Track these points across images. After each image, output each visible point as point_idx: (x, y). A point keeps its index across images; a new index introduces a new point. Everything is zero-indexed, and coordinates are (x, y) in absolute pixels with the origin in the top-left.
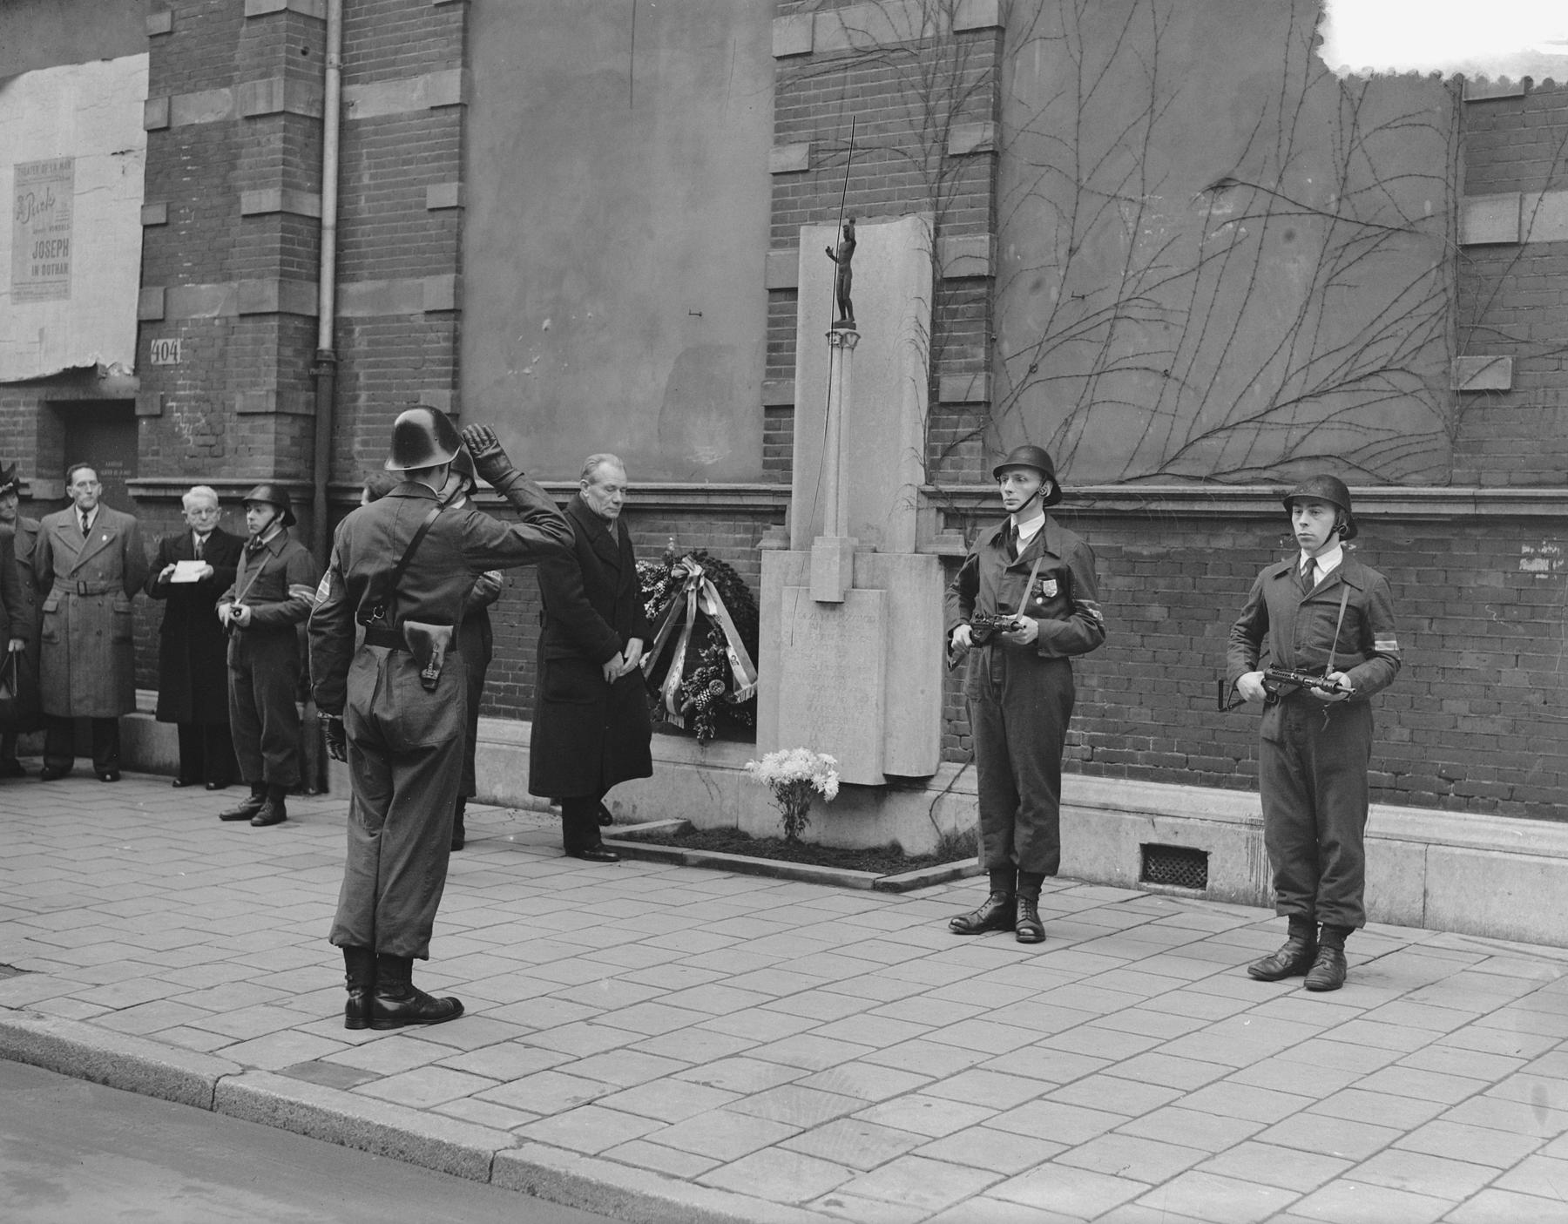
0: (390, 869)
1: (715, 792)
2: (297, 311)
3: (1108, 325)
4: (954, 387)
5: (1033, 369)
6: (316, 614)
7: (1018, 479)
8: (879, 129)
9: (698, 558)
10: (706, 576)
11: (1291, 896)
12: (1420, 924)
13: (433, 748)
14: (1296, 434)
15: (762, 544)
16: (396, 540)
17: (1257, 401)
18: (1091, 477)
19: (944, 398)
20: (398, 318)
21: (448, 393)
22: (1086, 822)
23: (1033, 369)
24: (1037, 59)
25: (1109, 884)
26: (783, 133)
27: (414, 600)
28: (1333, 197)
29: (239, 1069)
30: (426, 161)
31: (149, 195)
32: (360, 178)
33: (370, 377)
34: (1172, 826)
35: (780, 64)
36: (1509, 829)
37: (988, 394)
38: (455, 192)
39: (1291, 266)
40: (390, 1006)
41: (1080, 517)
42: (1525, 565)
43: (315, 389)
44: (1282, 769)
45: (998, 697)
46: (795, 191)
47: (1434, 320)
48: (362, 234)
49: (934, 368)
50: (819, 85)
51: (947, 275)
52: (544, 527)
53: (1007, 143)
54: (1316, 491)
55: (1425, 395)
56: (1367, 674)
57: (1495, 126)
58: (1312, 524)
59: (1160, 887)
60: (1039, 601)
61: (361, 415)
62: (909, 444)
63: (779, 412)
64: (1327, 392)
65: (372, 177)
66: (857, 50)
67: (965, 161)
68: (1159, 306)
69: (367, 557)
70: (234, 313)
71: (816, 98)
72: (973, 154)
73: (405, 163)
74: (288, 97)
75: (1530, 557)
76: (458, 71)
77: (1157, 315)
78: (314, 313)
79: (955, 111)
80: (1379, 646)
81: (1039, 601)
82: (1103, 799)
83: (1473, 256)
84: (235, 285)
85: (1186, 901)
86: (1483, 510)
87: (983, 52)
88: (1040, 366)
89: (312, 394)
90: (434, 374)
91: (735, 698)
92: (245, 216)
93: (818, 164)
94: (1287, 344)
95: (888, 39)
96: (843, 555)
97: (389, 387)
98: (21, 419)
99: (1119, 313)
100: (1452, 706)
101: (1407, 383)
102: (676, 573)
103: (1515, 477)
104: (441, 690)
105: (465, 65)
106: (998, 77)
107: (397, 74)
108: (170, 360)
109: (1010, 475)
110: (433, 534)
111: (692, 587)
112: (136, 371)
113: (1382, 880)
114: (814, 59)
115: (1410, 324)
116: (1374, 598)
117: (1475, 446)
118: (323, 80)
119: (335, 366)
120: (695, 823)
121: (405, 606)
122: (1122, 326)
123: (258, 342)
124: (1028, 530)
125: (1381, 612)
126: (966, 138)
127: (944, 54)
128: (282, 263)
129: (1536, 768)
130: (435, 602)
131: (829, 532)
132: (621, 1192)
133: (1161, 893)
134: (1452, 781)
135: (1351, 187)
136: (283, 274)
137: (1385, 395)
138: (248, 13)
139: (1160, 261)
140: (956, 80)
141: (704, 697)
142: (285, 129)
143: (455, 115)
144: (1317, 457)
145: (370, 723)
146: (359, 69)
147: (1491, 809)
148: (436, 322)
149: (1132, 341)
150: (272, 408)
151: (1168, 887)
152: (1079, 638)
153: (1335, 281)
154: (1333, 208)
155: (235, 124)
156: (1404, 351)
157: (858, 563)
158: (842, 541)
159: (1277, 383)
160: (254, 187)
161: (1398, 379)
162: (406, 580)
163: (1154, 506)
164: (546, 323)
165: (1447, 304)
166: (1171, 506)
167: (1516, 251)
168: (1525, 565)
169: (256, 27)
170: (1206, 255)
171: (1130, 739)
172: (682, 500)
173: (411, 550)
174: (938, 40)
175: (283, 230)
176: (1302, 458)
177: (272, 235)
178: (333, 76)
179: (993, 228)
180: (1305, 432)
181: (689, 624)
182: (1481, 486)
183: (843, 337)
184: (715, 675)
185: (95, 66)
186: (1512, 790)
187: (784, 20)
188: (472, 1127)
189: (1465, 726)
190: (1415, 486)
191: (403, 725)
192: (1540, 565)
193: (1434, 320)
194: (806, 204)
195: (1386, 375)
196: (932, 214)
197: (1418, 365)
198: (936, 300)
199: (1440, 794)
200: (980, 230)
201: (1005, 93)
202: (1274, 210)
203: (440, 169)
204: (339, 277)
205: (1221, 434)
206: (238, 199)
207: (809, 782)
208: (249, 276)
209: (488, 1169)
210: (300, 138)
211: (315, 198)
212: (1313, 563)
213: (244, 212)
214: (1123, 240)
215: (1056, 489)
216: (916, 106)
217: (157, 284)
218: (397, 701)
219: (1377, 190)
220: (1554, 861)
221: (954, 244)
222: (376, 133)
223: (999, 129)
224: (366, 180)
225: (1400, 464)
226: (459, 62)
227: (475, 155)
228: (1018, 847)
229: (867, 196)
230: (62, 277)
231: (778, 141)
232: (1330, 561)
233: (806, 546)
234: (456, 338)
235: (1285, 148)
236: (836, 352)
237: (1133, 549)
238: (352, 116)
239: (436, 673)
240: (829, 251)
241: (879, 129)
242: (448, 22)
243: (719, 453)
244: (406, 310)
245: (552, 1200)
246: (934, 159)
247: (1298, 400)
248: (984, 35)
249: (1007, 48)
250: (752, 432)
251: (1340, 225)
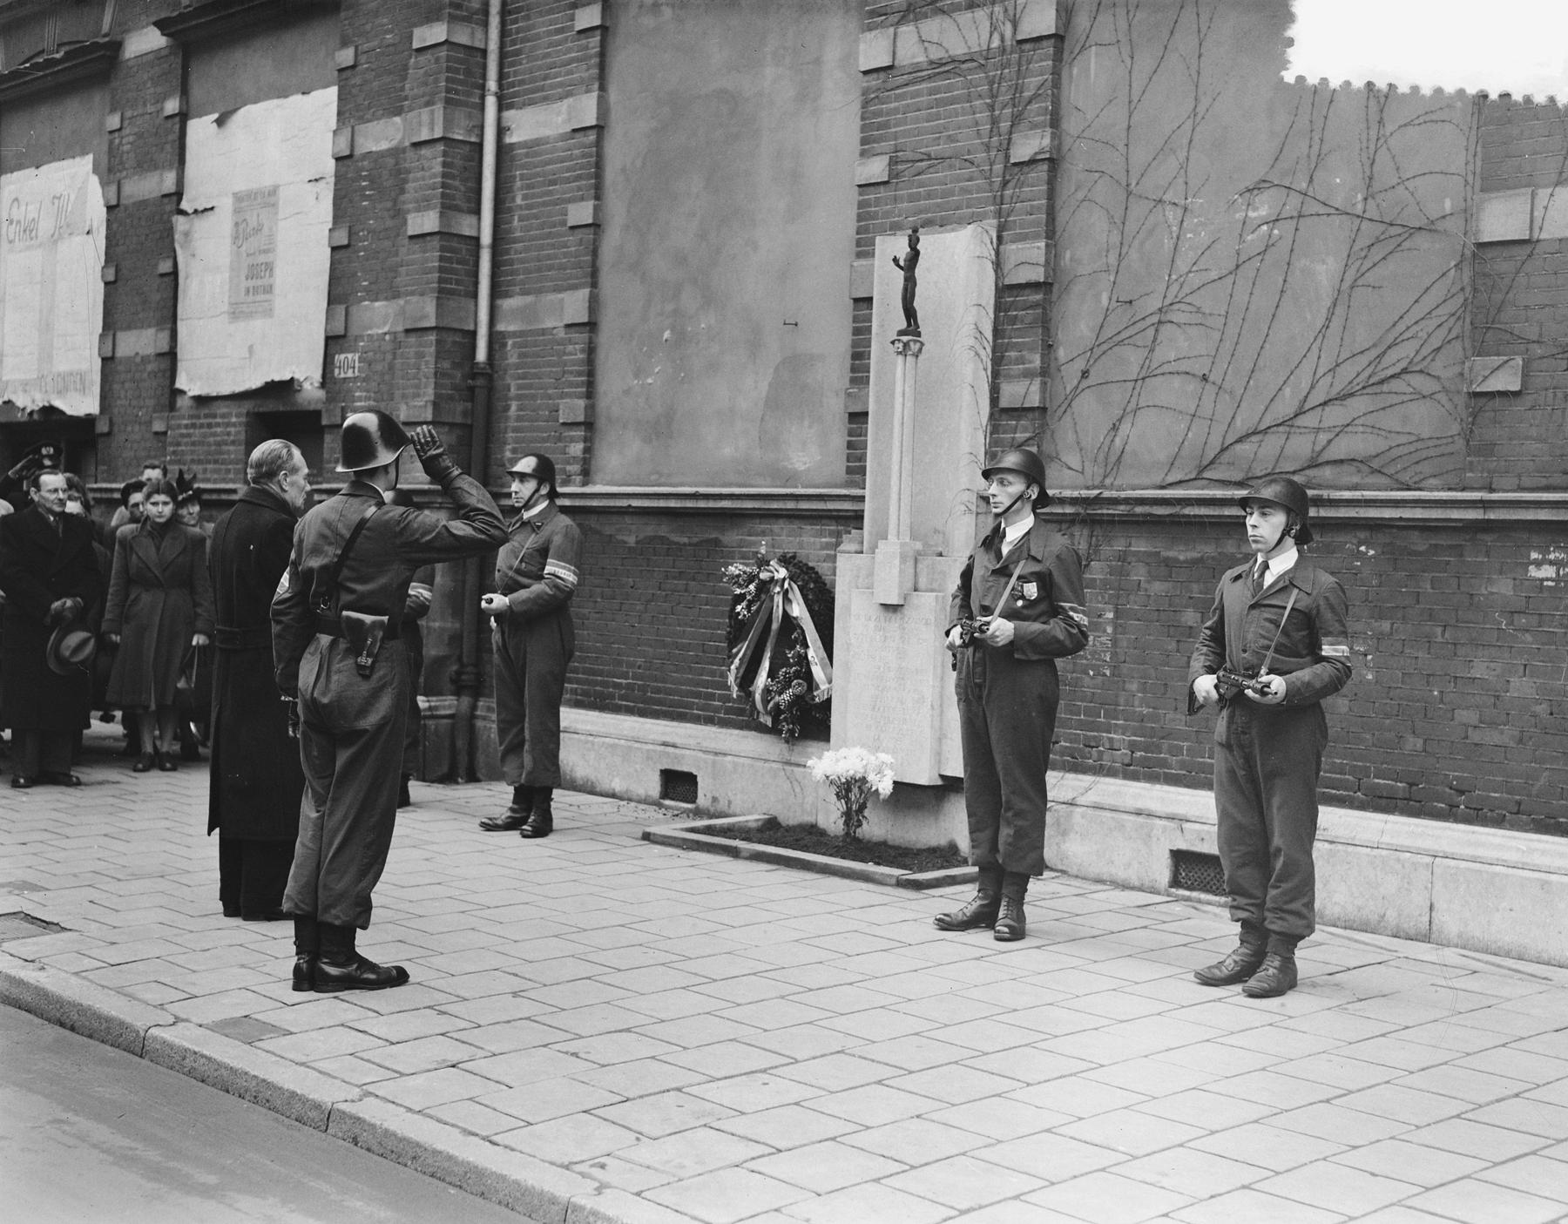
0: (330, 844)
1: (798, 790)
2: (456, 325)
3: (1151, 332)
4: (1013, 393)
5: (1085, 374)
6: (278, 603)
7: (1001, 482)
8: (951, 139)
9: (785, 561)
10: (791, 578)
11: (1242, 901)
12: (1425, 937)
13: (366, 731)
14: (1323, 438)
15: (842, 547)
16: (337, 534)
17: (1285, 408)
18: (1136, 482)
19: (1004, 403)
20: (543, 332)
21: (581, 403)
22: (1121, 827)
23: (1085, 374)
24: (1093, 66)
25: (1140, 889)
26: (867, 146)
27: (352, 591)
28: (1360, 197)
29: (172, 1020)
30: (568, 180)
31: (337, 218)
32: (513, 199)
33: (519, 387)
34: (1199, 832)
35: (867, 78)
36: (1514, 843)
37: (1043, 399)
38: (591, 210)
39: (1321, 268)
40: (333, 971)
41: (1121, 522)
42: (1534, 572)
43: (472, 399)
44: (1232, 773)
45: (980, 697)
46: (877, 202)
47: (1453, 320)
48: (517, 252)
49: (996, 375)
50: (898, 98)
51: (1007, 282)
52: (477, 524)
53: (1065, 148)
54: (1268, 493)
55: (1442, 397)
56: (1307, 679)
57: (1509, 122)
58: (1265, 526)
59: (1187, 893)
60: (1020, 603)
61: (512, 424)
62: (968, 450)
63: (858, 418)
64: (1352, 395)
65: (525, 197)
66: (932, 62)
67: (1026, 169)
68: (1199, 310)
69: (316, 551)
70: (400, 328)
71: (896, 111)
72: (1033, 162)
73: (553, 183)
74: (448, 123)
75: (1538, 564)
76: (595, 94)
77: (1197, 318)
78: (471, 328)
79: (1016, 120)
80: (1327, 650)
81: (1020, 603)
82: (1140, 804)
83: (1489, 253)
84: (401, 302)
85: (1209, 908)
86: (1492, 515)
87: (1042, 62)
88: (1092, 372)
89: (469, 405)
90: (571, 385)
91: (813, 698)
92: (411, 237)
93: (897, 176)
94: (1315, 348)
95: (959, 50)
96: (903, 559)
97: (534, 397)
98: (232, 430)
99: (1164, 318)
100: (1464, 716)
101: (1426, 385)
102: (764, 576)
103: (1526, 482)
104: (375, 677)
105: (602, 88)
106: (1057, 84)
107: (545, 99)
108: (350, 374)
109: (995, 478)
110: (369, 529)
111: (778, 589)
112: (323, 385)
113: (1334, 889)
114: (895, 72)
115: (1431, 324)
116: (1322, 603)
117: (1487, 449)
118: (482, 107)
119: (490, 378)
120: (781, 819)
121: (346, 598)
122: (1166, 330)
123: (420, 355)
124: (1014, 532)
125: (1328, 615)
126: (1027, 146)
127: (1007, 65)
128: (441, 280)
129: (1542, 781)
130: (371, 593)
131: (892, 537)
132: (418, 1145)
133: (1188, 899)
134: (1462, 792)
135: (1376, 186)
136: (440, 291)
137: (1406, 398)
138: (415, 45)
139: (1201, 265)
140: (1018, 89)
141: (786, 696)
142: (445, 154)
143: (592, 137)
144: (1342, 461)
145: (313, 705)
146: (515, 95)
147: (1499, 822)
148: (575, 336)
149: (1176, 345)
150: (430, 418)
151: (1195, 894)
152: (1058, 641)
153: (1360, 282)
154: (1359, 208)
155: (404, 150)
156: (1424, 352)
157: (920, 566)
158: (903, 545)
159: (1305, 386)
160: (418, 210)
161: (1417, 381)
162: (346, 572)
163: (1188, 511)
164: (667, 335)
165: (1465, 304)
166: (1203, 511)
167: (1522, 252)
168: (1534, 572)
169: (422, 58)
170: (1243, 258)
171: (1165, 744)
172: (775, 505)
173: (349, 545)
174: (1002, 50)
175: (442, 249)
176: (1328, 463)
177: (432, 257)
178: (491, 102)
179: (1051, 233)
180: (1330, 436)
181: (775, 626)
182: (1492, 490)
183: (906, 345)
184: (797, 675)
185: (297, 99)
186: (1519, 803)
187: (869, 35)
188: (330, 1081)
189: (1476, 737)
190: (1431, 490)
191: (338, 706)
192: (1548, 572)
193: (1453, 320)
194: (887, 214)
195: (1407, 377)
196: (995, 222)
197: (1437, 367)
198: (999, 307)
199: (1452, 806)
200: (1036, 237)
201: (1064, 103)
202: (1306, 211)
203: (579, 189)
204: (496, 292)
205: (1254, 439)
206: (405, 222)
207: (864, 780)
208: (412, 293)
209: (325, 1119)
210: (458, 162)
211: (472, 219)
212: (1266, 566)
213: (410, 233)
214: (1168, 244)
215: (1043, 493)
216: (983, 116)
217: (340, 303)
218: (333, 686)
219: (1401, 187)
220: (1553, 877)
221: (1015, 251)
222: (527, 155)
223: (1057, 136)
224: (519, 201)
225: (1418, 468)
226: (596, 86)
227: (611, 174)
228: (1001, 847)
229: (938, 205)
230: (267, 296)
231: (863, 154)
232: (1284, 561)
233: (873, 550)
234: (591, 350)
235: (1316, 148)
236: (900, 358)
237: (1171, 554)
238: (508, 140)
239: (370, 661)
240: (895, 260)
241: (951, 139)
242: (587, 48)
243: (809, 459)
244: (549, 324)
245: (369, 1150)
246: (998, 167)
247: (1325, 403)
248: (1045, 43)
249: (1066, 55)
250: (838, 440)
251: (1365, 225)
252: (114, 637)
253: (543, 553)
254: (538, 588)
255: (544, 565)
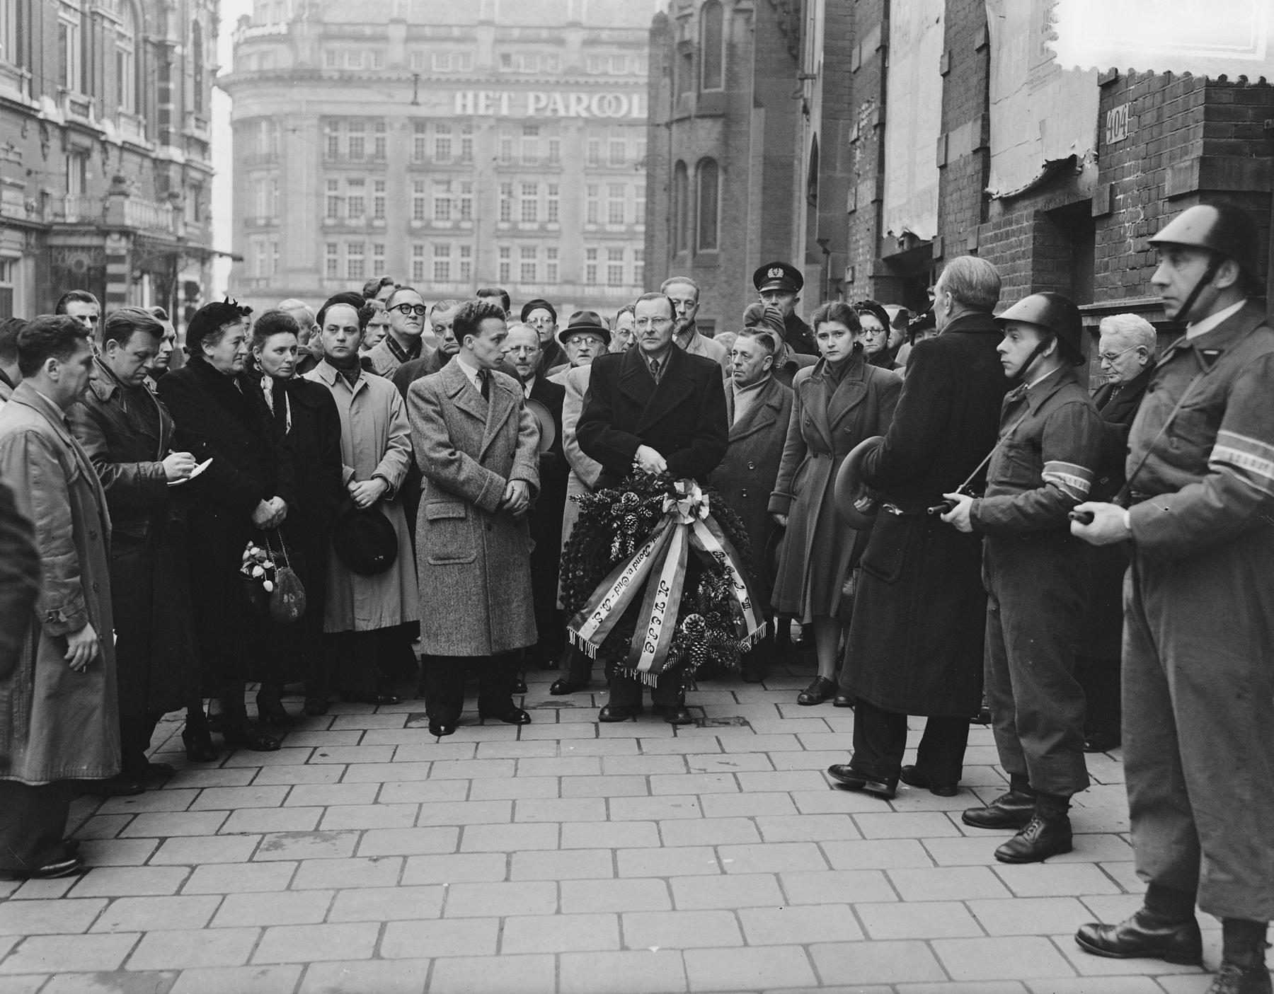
252: (780, 517)
253: (1211, 415)
254: (1198, 492)
255: (1212, 441)
